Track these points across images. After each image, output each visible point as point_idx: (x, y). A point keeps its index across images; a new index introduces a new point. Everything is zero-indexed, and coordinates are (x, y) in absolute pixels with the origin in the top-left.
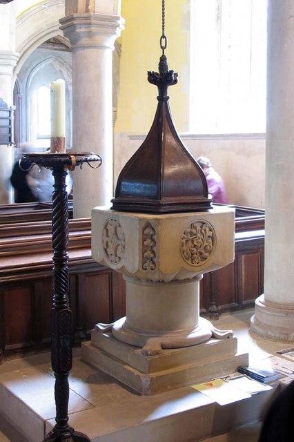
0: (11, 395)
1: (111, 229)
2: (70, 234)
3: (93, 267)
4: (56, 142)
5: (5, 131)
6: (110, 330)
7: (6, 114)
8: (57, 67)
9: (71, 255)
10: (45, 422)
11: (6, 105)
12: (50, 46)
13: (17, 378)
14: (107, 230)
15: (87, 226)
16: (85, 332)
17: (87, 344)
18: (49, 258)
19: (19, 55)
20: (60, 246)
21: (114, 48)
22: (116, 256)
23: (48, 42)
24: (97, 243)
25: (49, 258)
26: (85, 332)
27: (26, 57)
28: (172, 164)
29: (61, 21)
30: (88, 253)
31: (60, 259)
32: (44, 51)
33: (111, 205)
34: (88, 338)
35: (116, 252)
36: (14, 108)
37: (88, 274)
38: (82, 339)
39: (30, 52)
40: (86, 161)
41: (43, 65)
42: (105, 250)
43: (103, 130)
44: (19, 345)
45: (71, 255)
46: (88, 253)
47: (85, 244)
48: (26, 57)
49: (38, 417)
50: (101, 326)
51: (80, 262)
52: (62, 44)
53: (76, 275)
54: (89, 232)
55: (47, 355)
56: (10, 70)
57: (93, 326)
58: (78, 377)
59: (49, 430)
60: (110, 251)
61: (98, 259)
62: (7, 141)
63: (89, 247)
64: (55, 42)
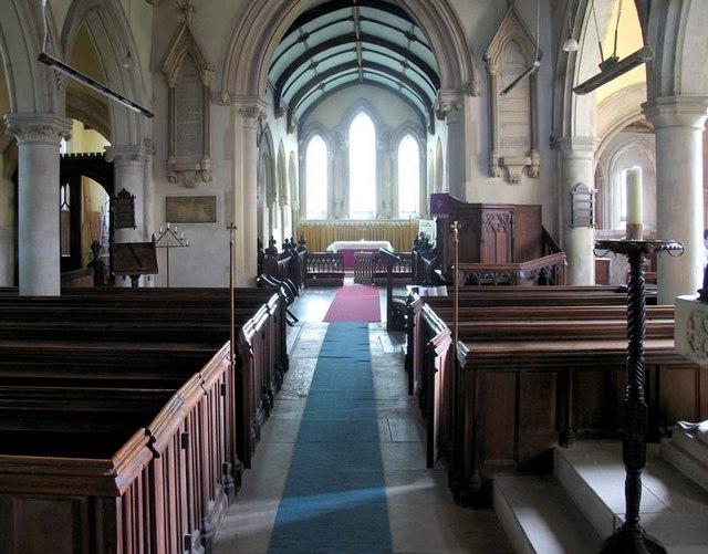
0: (581, 480)
1: (698, 321)
2: (647, 322)
3: (677, 359)
4: (633, 228)
5: (587, 214)
6: (695, 431)
7: (588, 197)
8: (641, 147)
9: (646, 344)
10: (615, 517)
11: (587, 189)
12: (634, 129)
13: (590, 463)
14: (693, 322)
15: (669, 314)
16: (666, 428)
17: (665, 441)
18: (624, 345)
19: (600, 141)
20: (635, 332)
21: (704, 129)
22: (703, 350)
23: (633, 125)
24: (681, 333)
25: (624, 345)
26: (666, 428)
27: (606, 143)
28: (392, 485)
29: (642, 105)
30: (670, 344)
31: (635, 348)
32: (627, 133)
33: (698, 295)
34: (669, 434)
35: (703, 345)
36: (595, 191)
37: (670, 366)
38: (663, 435)
39: (615, 134)
40: (665, 248)
41: (626, 149)
42: (691, 343)
43: (692, 214)
44: (506, 462)
45: (646, 344)
46: (670, 344)
47: (667, 333)
48: (606, 143)
49: (609, 510)
50: (684, 425)
51: (653, 353)
52: (645, 126)
53: (657, 366)
54: (673, 321)
55: (619, 446)
56: (591, 155)
57: (674, 423)
58: (653, 474)
59: (619, 525)
60: (696, 344)
61: (684, 349)
62: (588, 224)
63: (672, 338)
64: (638, 126)
